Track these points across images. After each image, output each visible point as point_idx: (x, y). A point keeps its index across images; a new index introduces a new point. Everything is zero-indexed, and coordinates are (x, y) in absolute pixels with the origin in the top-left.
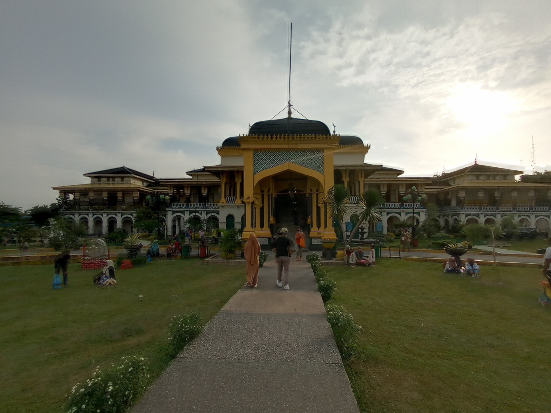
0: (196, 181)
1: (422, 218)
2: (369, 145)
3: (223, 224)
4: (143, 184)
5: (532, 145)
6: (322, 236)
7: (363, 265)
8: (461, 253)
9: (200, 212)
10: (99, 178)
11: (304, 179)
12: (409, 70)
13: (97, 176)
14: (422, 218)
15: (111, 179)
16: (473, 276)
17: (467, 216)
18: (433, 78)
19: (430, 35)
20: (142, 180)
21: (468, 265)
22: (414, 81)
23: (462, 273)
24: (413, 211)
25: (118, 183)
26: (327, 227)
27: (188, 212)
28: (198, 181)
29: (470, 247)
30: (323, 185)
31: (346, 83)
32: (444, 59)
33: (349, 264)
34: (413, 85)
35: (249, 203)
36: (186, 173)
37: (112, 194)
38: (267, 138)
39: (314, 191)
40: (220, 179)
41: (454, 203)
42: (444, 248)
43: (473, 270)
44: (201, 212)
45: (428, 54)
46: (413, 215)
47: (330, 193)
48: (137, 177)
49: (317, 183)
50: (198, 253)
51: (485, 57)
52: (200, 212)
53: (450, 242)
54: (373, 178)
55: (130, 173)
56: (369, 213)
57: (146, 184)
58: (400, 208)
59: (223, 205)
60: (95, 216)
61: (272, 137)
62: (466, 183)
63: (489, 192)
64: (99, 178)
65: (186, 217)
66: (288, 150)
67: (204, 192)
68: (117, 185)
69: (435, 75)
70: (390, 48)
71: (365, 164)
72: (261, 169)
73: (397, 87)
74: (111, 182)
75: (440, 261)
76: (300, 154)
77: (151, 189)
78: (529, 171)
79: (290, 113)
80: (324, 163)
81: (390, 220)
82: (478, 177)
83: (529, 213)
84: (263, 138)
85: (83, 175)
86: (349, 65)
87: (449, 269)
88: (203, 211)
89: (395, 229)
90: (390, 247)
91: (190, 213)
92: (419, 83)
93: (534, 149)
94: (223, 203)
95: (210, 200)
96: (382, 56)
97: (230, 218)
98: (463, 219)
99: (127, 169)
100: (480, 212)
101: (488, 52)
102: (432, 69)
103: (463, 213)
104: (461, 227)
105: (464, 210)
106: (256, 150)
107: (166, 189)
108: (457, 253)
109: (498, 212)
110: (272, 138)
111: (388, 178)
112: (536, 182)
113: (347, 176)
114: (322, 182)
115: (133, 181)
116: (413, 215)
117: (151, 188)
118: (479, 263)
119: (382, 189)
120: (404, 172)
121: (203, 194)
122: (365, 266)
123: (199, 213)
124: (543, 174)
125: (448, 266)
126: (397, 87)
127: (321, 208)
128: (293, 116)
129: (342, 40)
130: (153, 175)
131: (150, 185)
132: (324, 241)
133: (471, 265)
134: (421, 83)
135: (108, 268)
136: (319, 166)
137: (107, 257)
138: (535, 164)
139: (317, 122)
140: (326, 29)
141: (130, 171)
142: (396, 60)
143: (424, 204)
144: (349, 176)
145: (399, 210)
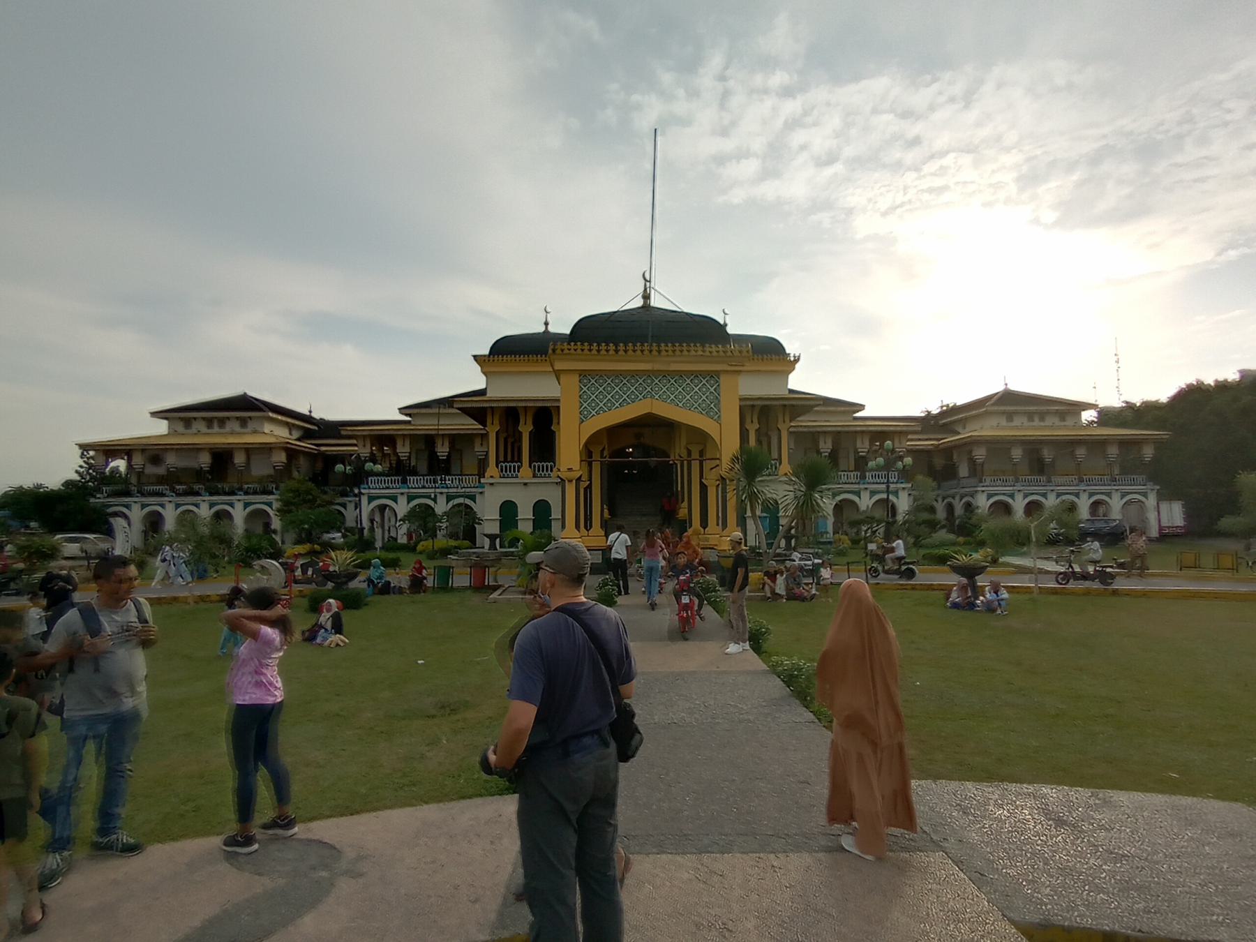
0: (437, 427)
1: (903, 504)
2: (797, 355)
3: (494, 522)
4: (291, 434)
5: (1116, 355)
6: (716, 545)
7: (802, 599)
8: (979, 570)
9: (433, 496)
10: (188, 423)
11: (668, 427)
12: (877, 175)
13: (181, 416)
14: (903, 504)
15: (216, 424)
16: (999, 612)
17: (990, 496)
18: (926, 196)
19: (920, 98)
20: (287, 424)
21: (990, 593)
22: (884, 204)
23: (978, 607)
24: (888, 487)
25: (232, 433)
26: (726, 527)
27: (406, 496)
28: (440, 427)
29: (995, 561)
30: (718, 443)
31: (738, 196)
32: (952, 156)
33: (775, 596)
34: (883, 210)
35: (570, 481)
36: (398, 411)
37: (222, 457)
38: (607, 351)
39: (695, 455)
40: (485, 425)
41: (963, 471)
42: (948, 563)
43: (998, 600)
44: (435, 496)
45: (916, 141)
46: (888, 496)
47: (735, 459)
48: (280, 417)
49: (701, 438)
50: (432, 585)
51: (1035, 157)
52: (433, 496)
53: (959, 551)
54: (806, 422)
55: (260, 410)
56: (811, 500)
57: (296, 434)
58: (859, 483)
59: (491, 481)
60: (147, 510)
61: (616, 347)
62: (988, 429)
63: (1033, 448)
64: (188, 423)
65: (402, 508)
66: (649, 374)
67: (442, 450)
68: (231, 436)
69: (931, 190)
70: (835, 121)
71: (791, 391)
72: (594, 413)
73: (850, 212)
74: (216, 429)
75: (941, 588)
76: (672, 381)
77: (309, 444)
78: (1112, 400)
79: (646, 297)
80: (719, 401)
81: (838, 508)
82: (1010, 416)
83: (1109, 488)
84: (599, 351)
85: (149, 415)
86: (742, 154)
87: (957, 600)
88: (438, 495)
89: (849, 530)
90: (848, 563)
91: (410, 498)
92: (898, 207)
93: (1119, 365)
94: (492, 477)
95: (455, 468)
96: (819, 139)
97: (508, 511)
98: (983, 503)
99: (254, 401)
100: (1015, 488)
101: (1041, 147)
102: (924, 176)
103: (983, 491)
104: (977, 526)
105: (985, 484)
106: (583, 374)
107: (355, 445)
108: (970, 572)
109: (1052, 488)
110: (617, 351)
111: (836, 422)
112: (1123, 425)
113: (755, 420)
114: (714, 434)
115: (267, 428)
116: (888, 496)
117: (309, 442)
118: (1011, 589)
119: (822, 445)
120: (866, 407)
121: (438, 456)
122: (804, 601)
123: (432, 499)
124: (1138, 405)
125: (955, 596)
126: (850, 212)
127: (709, 488)
128: (656, 302)
129: (726, 95)
130: (310, 412)
131: (307, 435)
132: (722, 555)
133: (996, 593)
134: (901, 205)
135: (331, 616)
136: (709, 405)
137: (288, 597)
138: (1121, 395)
139: (703, 319)
140: (690, 66)
141: (262, 406)
142: (849, 151)
143: (906, 475)
144: (759, 419)
145: (857, 486)
